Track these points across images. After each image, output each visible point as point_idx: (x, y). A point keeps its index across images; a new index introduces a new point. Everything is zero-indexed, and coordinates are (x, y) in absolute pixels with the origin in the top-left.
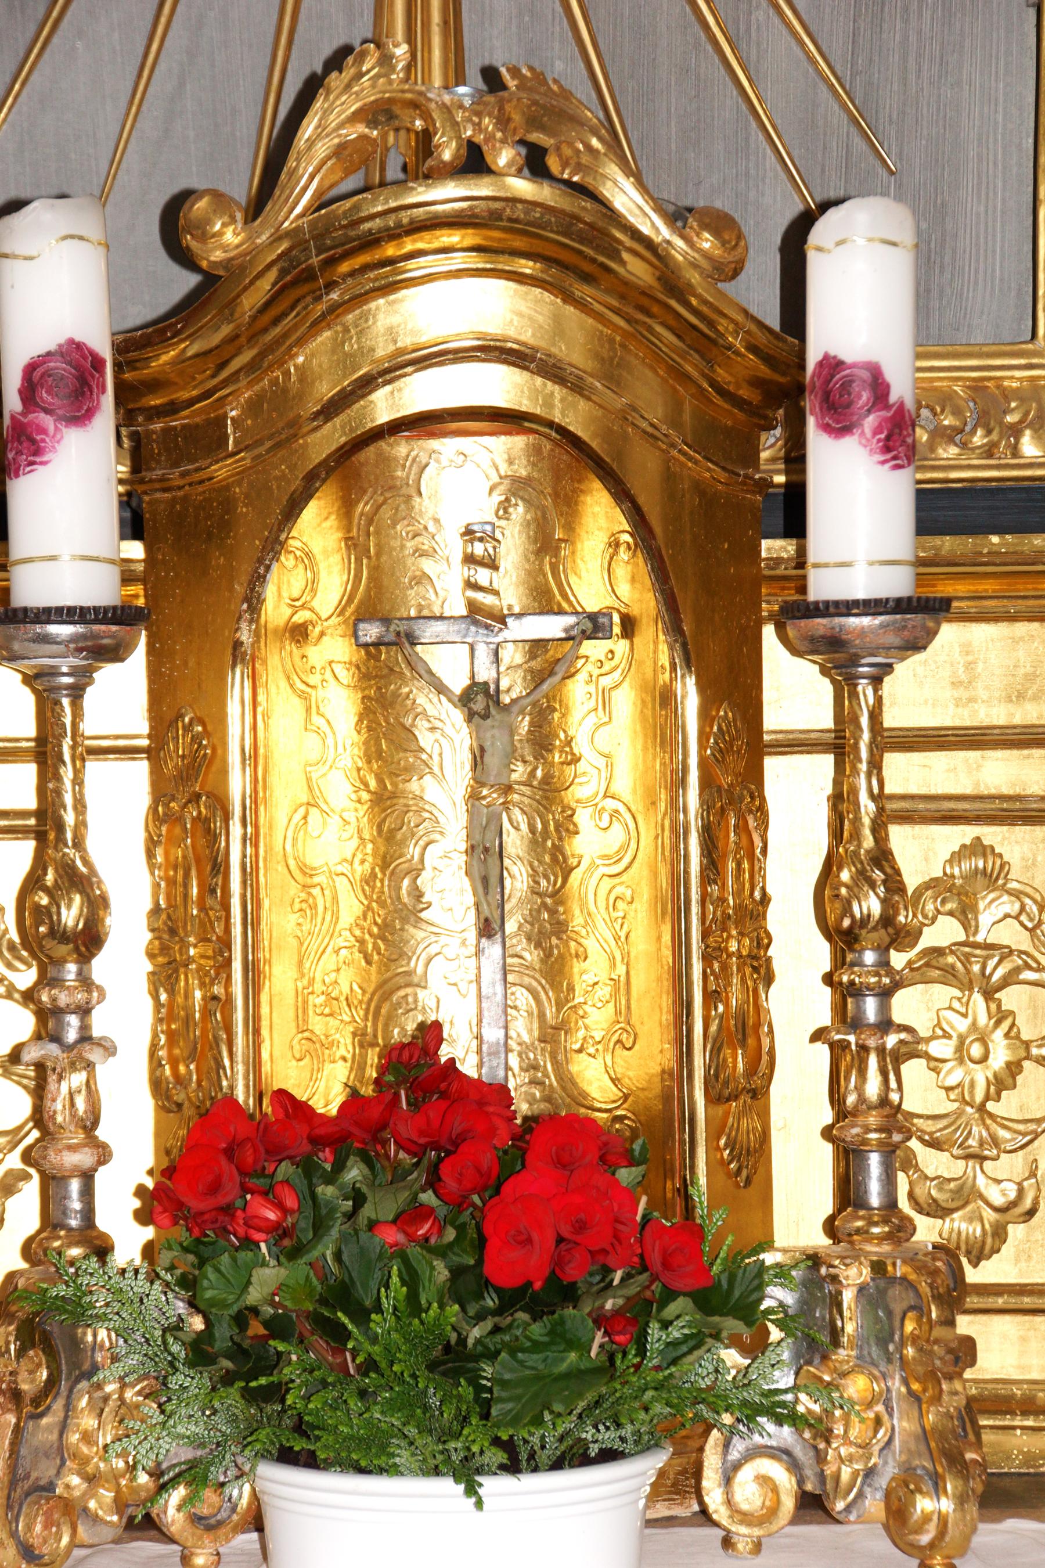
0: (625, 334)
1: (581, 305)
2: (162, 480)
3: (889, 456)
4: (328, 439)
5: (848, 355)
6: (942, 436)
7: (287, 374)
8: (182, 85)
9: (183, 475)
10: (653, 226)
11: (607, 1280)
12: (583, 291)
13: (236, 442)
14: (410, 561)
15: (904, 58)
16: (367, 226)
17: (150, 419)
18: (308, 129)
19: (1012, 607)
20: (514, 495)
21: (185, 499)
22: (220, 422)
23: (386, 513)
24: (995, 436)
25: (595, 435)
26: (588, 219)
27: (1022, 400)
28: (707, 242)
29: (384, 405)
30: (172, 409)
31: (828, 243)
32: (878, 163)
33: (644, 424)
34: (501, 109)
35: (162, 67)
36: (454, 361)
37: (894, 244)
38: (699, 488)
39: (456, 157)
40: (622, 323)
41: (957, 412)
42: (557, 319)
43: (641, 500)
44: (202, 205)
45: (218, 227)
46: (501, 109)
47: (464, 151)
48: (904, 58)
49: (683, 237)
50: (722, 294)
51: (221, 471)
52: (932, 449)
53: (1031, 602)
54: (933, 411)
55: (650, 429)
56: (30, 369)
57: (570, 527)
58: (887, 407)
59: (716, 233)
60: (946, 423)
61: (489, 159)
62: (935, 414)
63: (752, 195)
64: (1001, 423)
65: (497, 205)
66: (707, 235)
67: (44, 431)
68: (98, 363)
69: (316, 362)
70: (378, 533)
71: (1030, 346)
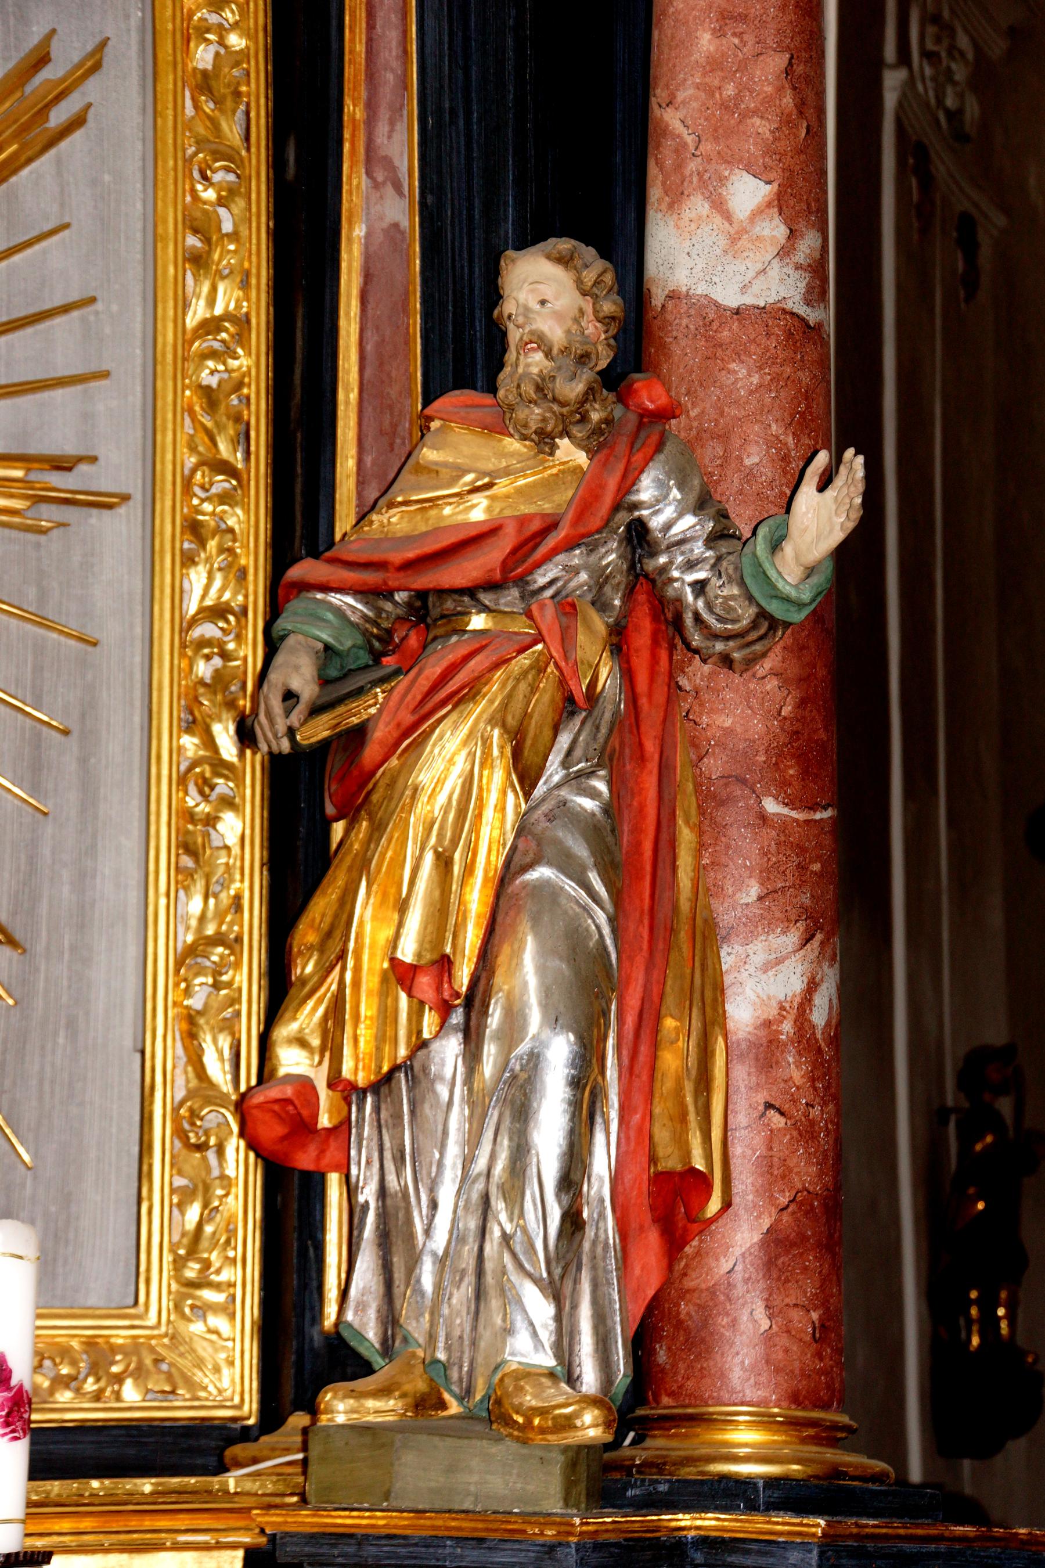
3: (8, 1430)
6: (61, 1382)
11: (39, 1223)
19: (107, 1540)
24: (102, 1383)
27: (126, 1354)
32: (17, 1160)
37: (21, 1257)
41: (74, 1363)
53: (122, 1537)
54: (53, 1360)
58: (9, 1389)
62: (55, 1364)
71: (132, 1311)
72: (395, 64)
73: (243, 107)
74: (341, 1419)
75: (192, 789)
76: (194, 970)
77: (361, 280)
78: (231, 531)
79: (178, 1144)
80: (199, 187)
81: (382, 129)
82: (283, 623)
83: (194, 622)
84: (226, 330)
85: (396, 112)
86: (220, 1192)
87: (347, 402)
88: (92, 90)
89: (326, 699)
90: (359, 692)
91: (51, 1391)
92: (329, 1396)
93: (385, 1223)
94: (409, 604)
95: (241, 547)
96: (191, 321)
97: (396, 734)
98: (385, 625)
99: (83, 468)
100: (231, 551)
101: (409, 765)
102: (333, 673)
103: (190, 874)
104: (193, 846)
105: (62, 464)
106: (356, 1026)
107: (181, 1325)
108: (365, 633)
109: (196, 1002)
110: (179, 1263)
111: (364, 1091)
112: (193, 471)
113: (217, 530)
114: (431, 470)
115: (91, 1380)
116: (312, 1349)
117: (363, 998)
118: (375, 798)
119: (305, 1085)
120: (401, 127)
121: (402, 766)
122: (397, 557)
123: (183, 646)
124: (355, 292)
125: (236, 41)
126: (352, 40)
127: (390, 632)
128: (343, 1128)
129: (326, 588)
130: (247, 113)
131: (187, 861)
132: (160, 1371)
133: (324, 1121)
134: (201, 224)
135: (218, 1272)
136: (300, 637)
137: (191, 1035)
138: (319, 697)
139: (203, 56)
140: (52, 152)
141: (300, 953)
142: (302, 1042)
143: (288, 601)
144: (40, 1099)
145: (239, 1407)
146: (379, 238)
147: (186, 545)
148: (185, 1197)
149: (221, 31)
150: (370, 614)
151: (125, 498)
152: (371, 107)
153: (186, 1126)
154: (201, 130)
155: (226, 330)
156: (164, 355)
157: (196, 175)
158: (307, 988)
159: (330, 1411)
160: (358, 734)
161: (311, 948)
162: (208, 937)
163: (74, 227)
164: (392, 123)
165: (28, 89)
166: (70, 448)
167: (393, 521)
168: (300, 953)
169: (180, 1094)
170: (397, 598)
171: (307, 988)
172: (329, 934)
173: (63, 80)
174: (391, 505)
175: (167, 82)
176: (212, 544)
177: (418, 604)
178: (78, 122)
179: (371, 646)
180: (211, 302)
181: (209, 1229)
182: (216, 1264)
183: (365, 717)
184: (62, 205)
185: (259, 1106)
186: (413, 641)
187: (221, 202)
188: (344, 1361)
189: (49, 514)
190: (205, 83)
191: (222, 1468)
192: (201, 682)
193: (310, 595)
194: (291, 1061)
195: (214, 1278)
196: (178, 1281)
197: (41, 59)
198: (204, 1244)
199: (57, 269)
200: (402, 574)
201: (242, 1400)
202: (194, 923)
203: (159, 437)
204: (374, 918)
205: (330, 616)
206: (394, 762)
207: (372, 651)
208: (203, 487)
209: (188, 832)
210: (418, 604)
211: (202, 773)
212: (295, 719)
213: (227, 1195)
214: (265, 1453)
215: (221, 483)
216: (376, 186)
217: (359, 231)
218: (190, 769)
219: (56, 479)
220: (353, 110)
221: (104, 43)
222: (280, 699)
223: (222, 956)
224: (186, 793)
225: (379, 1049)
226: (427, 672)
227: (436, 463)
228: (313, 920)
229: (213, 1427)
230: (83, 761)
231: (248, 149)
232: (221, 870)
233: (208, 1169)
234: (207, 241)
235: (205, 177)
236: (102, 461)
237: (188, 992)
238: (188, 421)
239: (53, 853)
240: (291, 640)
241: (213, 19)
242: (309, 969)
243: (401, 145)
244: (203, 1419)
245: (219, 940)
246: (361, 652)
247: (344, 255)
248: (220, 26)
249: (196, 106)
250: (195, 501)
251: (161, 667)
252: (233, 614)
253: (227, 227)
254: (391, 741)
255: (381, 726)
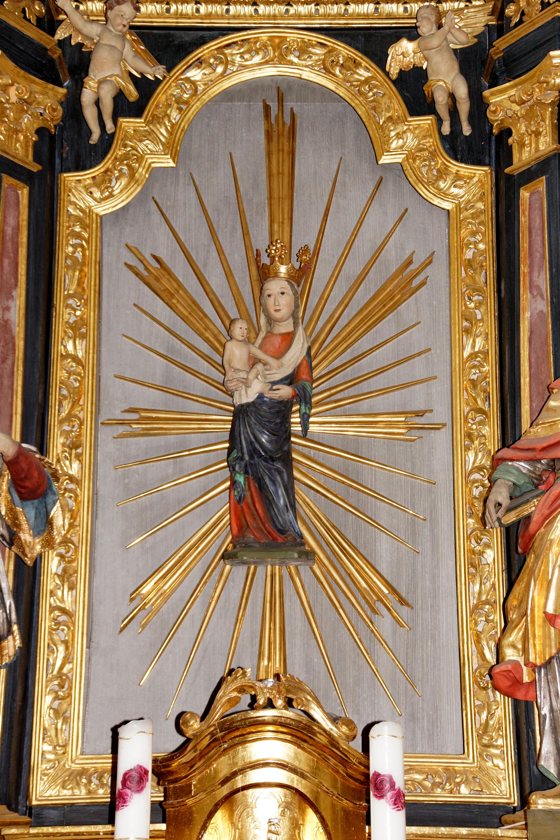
0: (318, 758)
1: (303, 749)
2: (172, 804)
4: (225, 790)
5: (382, 773)
7: (211, 770)
8: (200, 666)
9: (178, 803)
10: (327, 725)
12: (305, 745)
13: (195, 792)
14: (252, 831)
15: (423, 661)
16: (235, 724)
17: (169, 784)
18: (220, 693)
20: (287, 808)
21: (179, 810)
22: (190, 785)
23: (245, 814)
24: (452, 786)
25: (308, 792)
26: (304, 722)
28: (344, 729)
29: (239, 782)
30: (176, 781)
31: (375, 736)
33: (324, 788)
34: (279, 688)
35: (194, 661)
36: (262, 767)
38: (344, 809)
39: (264, 703)
40: (317, 755)
41: (440, 777)
42: (296, 754)
43: (323, 814)
44: (188, 716)
45: (192, 723)
46: (279, 688)
47: (266, 701)
48: (423, 661)
49: (336, 727)
50: (349, 747)
51: (190, 802)
52: (432, 790)
55: (326, 790)
56: (125, 774)
57: (303, 820)
58: (394, 790)
59: (347, 726)
60: (437, 781)
61: (274, 703)
63: (376, 701)
64: (454, 782)
65: (276, 718)
66: (344, 727)
67: (127, 795)
68: (146, 772)
69: (222, 766)
70: (242, 821)
71: (463, 756)
72: (540, 249)
73: (484, 271)
74: (540, 807)
75: (473, 541)
76: (478, 614)
77: (529, 334)
78: (484, 436)
79: (476, 687)
80: (468, 303)
81: (535, 274)
82: (496, 475)
83: (471, 472)
84: (480, 357)
85: (541, 267)
86: (494, 707)
87: (524, 382)
88: (429, 271)
89: (513, 505)
90: (527, 501)
91: (432, 789)
92: (534, 797)
93: (554, 723)
94: (548, 464)
95: (489, 442)
96: (466, 354)
97: (542, 518)
98: (538, 473)
99: (427, 414)
100: (484, 444)
101: (547, 532)
102: (517, 494)
103: (474, 576)
104: (475, 563)
105: (419, 414)
106: (534, 640)
107: (483, 763)
108: (530, 477)
109: (480, 628)
110: (480, 737)
111: (540, 667)
112: (468, 413)
113: (479, 436)
114: (554, 410)
115: (448, 784)
116: (534, 775)
117: (536, 628)
118: (536, 545)
119: (516, 664)
120: (543, 273)
121: (546, 531)
122: (539, 446)
123: (467, 483)
124: (526, 339)
125: (481, 246)
126: (523, 242)
127: (541, 476)
128: (533, 683)
129: (512, 460)
130: (486, 273)
131: (472, 570)
132: (476, 782)
133: (526, 679)
134: (468, 317)
135: (496, 741)
136: (502, 480)
137: (478, 641)
138: (510, 504)
139: (469, 254)
140: (414, 296)
141: (511, 609)
142: (514, 647)
143: (498, 465)
144: (423, 668)
145: (510, 798)
146: (535, 317)
147: (466, 443)
148: (480, 709)
149: (476, 243)
150: (531, 469)
151: (444, 425)
152: (531, 267)
153: (479, 680)
154: (468, 281)
155: (480, 357)
156: (455, 368)
157: (467, 299)
158: (514, 624)
159: (536, 803)
160: (528, 518)
161: (515, 607)
162: (483, 601)
163: (422, 323)
164: (539, 272)
165: (404, 274)
166: (422, 408)
167: (539, 431)
168: (511, 609)
169: (475, 667)
170: (542, 461)
171: (514, 624)
172: (521, 602)
173: (417, 269)
174: (537, 425)
175: (454, 266)
176: (476, 442)
177: (552, 463)
178: (423, 284)
179: (533, 482)
180: (473, 346)
181: (491, 723)
182: (495, 737)
183: (530, 511)
184: (418, 315)
185: (497, 673)
186: (551, 479)
187: (476, 307)
188: (544, 784)
189: (414, 435)
190: (469, 264)
191: (500, 824)
192: (475, 498)
193: (506, 463)
194: (510, 654)
195: (494, 743)
196: (480, 744)
197: (409, 262)
198: (490, 729)
199: (416, 339)
200: (541, 453)
201: (510, 795)
202: (476, 595)
203: (454, 401)
204: (538, 595)
205: (514, 471)
206: (542, 530)
207: (534, 484)
208: (472, 419)
209: (472, 558)
210: (552, 463)
211: (477, 534)
212: (500, 514)
213: (497, 708)
214: (517, 819)
215: (479, 418)
216: (534, 297)
217: (528, 315)
218: (471, 533)
219: (417, 420)
220: (524, 269)
221: (433, 253)
222: (493, 506)
223: (488, 609)
224: (471, 542)
225: (544, 649)
226: (553, 492)
227: (555, 407)
228: (515, 596)
229: (500, 806)
230: (432, 530)
231: (486, 286)
232: (487, 573)
233: (489, 698)
234: (471, 323)
235: (470, 299)
236: (435, 411)
237: (476, 624)
238: (465, 393)
239: (422, 568)
240: (498, 482)
241: (472, 240)
242: (514, 616)
243: (543, 280)
244: (495, 803)
245: (487, 602)
246: (529, 485)
247: (521, 325)
248: (475, 242)
249: (466, 273)
250: (470, 425)
251: (458, 492)
252: (486, 469)
253: (479, 317)
254: (540, 521)
255: (536, 515)
